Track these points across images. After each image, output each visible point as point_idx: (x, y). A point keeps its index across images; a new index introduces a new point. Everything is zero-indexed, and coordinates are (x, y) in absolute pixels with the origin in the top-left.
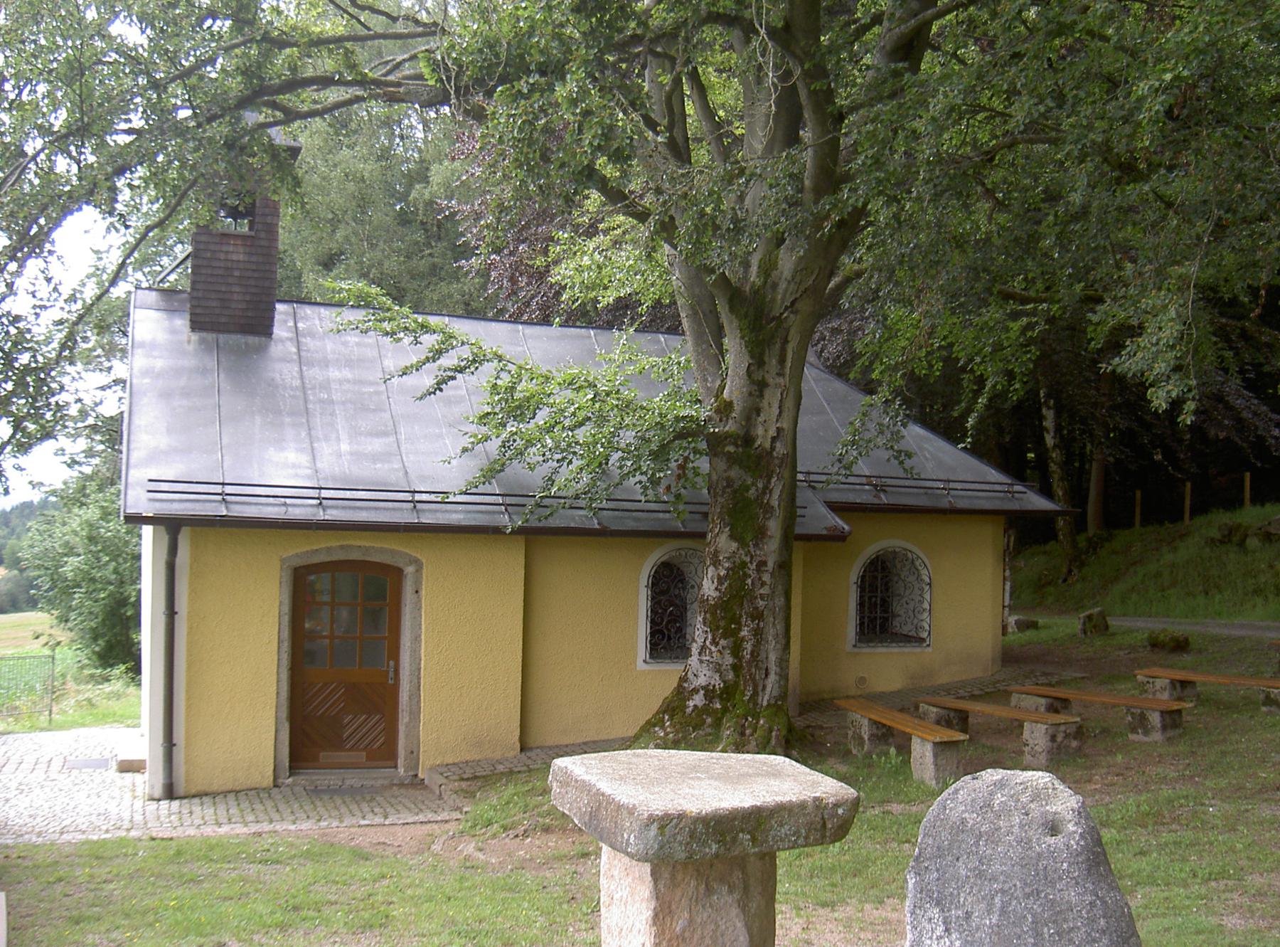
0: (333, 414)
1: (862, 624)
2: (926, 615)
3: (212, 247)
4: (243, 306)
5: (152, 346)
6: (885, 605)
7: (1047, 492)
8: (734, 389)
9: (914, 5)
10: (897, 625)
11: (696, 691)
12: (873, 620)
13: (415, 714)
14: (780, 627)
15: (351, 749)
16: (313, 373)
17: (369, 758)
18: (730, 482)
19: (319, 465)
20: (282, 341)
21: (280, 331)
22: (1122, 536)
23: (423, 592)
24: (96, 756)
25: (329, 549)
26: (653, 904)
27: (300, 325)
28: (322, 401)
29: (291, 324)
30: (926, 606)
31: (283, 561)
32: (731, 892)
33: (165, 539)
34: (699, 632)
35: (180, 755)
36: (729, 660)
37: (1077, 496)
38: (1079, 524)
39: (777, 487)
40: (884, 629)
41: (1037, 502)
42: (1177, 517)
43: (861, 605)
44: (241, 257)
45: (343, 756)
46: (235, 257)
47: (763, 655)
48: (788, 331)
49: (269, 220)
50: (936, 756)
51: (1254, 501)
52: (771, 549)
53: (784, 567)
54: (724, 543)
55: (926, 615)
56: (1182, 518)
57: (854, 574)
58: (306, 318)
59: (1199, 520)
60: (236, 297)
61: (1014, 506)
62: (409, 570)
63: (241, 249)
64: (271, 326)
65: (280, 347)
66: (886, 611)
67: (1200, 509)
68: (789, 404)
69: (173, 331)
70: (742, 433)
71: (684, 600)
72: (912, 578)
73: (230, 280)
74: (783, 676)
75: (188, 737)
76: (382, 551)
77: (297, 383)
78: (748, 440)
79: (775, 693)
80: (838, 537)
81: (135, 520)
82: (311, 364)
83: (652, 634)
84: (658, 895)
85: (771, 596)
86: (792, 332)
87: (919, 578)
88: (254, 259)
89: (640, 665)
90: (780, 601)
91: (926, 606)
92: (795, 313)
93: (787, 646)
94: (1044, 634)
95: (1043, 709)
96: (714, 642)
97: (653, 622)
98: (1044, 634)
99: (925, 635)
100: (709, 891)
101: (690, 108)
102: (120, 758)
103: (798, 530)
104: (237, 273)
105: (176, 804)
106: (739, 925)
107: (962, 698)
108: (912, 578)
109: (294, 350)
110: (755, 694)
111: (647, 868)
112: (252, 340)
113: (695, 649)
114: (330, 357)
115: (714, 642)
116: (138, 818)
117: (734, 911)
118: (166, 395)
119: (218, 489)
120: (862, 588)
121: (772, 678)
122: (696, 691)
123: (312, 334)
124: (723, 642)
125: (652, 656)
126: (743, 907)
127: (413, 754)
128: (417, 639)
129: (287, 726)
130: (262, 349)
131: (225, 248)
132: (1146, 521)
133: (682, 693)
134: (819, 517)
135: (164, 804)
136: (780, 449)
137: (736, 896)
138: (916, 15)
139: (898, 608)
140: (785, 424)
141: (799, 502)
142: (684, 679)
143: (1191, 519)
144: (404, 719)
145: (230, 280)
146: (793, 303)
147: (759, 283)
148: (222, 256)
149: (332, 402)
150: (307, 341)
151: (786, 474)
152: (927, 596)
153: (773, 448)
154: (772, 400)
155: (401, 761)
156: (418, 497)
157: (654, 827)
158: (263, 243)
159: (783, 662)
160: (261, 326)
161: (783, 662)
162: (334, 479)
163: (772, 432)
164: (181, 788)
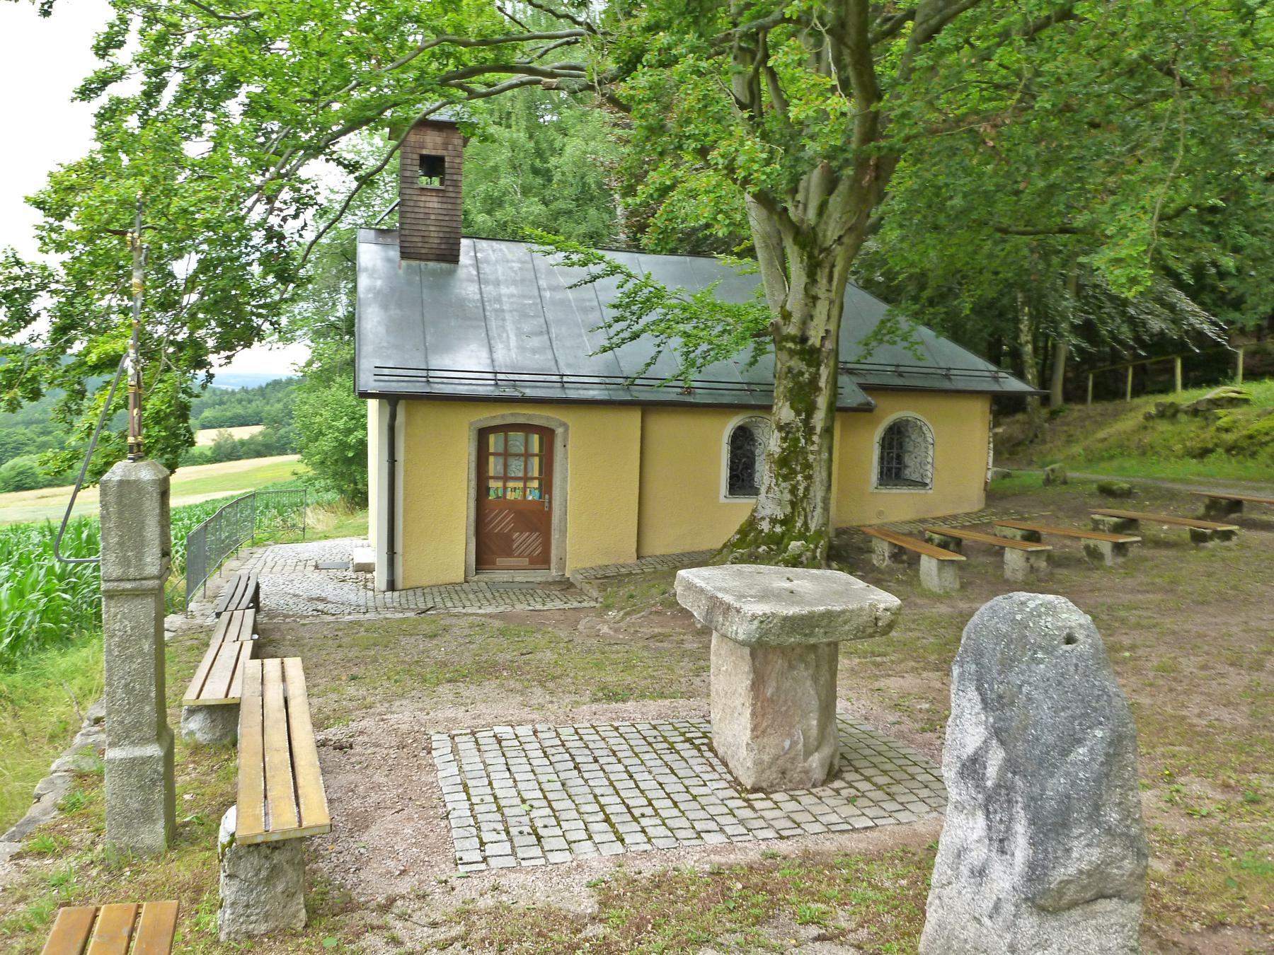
0: (503, 320)
1: (881, 473)
2: (929, 466)
3: (415, 198)
4: (438, 241)
5: (372, 273)
6: (899, 458)
7: (1020, 375)
8: (795, 303)
9: (941, 4)
10: (907, 473)
11: (763, 518)
12: (889, 470)
13: (563, 532)
14: (824, 475)
15: (518, 556)
16: (489, 290)
17: (531, 562)
18: (790, 370)
19: (495, 356)
20: (466, 266)
21: (465, 258)
22: (1076, 410)
23: (569, 447)
24: (338, 560)
25: (503, 416)
26: (751, 676)
27: (479, 255)
28: (496, 310)
29: (472, 254)
30: (930, 460)
31: (471, 424)
32: (806, 669)
33: (387, 409)
34: (764, 473)
35: (399, 561)
36: (788, 497)
37: (1044, 381)
38: (1046, 400)
39: (824, 372)
40: (898, 476)
41: (1013, 384)
42: (1118, 394)
43: (882, 458)
44: (436, 205)
45: (511, 561)
46: (431, 205)
47: (812, 494)
48: (835, 257)
49: (455, 177)
50: (940, 570)
51: (1185, 386)
52: (819, 419)
53: (828, 431)
54: (785, 413)
55: (929, 466)
56: (1123, 395)
57: (878, 433)
58: (482, 250)
59: (1137, 401)
60: (432, 234)
61: (996, 388)
62: (559, 431)
63: (435, 199)
64: (458, 256)
65: (465, 270)
66: (900, 463)
67: (1139, 391)
68: (835, 312)
69: (389, 260)
70: (799, 334)
71: (753, 453)
72: (920, 440)
73: (428, 222)
74: (826, 509)
75: (404, 547)
76: (541, 417)
77: (478, 297)
78: (804, 339)
79: (821, 522)
80: (866, 409)
81: (365, 395)
82: (487, 283)
83: (731, 478)
84: (755, 670)
85: (819, 452)
86: (838, 259)
87: (925, 440)
88: (445, 206)
89: (722, 500)
90: (825, 455)
91: (930, 460)
92: (841, 244)
93: (829, 488)
94: (1017, 482)
95: (1018, 538)
96: (777, 484)
97: (732, 469)
98: (1017, 482)
99: (928, 481)
100: (791, 667)
101: (763, 86)
102: (356, 561)
103: (839, 404)
104: (433, 217)
105: (396, 594)
106: (812, 692)
107: (955, 528)
108: (920, 440)
109: (475, 273)
110: (805, 523)
111: (747, 651)
112: (444, 266)
113: (763, 490)
114: (501, 278)
115: (777, 484)
116: (371, 604)
117: (809, 683)
118: (385, 307)
119: (424, 373)
120: (883, 447)
121: (819, 511)
122: (763, 518)
123: (487, 262)
124: (784, 485)
125: (731, 493)
126: (815, 679)
127: (562, 560)
128: (565, 479)
129: (474, 540)
130: (452, 273)
131: (423, 198)
132: (1097, 398)
133: (752, 523)
134: (852, 394)
135: (389, 594)
136: (829, 345)
137: (811, 671)
138: (940, 11)
139: (908, 460)
140: (832, 327)
141: (839, 384)
142: (755, 510)
143: (1132, 397)
144: (555, 536)
145: (428, 222)
146: (840, 237)
147: (812, 223)
148: (422, 204)
149: (503, 311)
150: (484, 266)
151: (832, 363)
152: (931, 453)
153: (822, 345)
154: (821, 309)
155: (552, 565)
156: (565, 379)
157: (756, 623)
158: (453, 195)
159: (826, 501)
160: (450, 256)
161: (826, 501)
162: (506, 366)
163: (822, 333)
164: (400, 583)
